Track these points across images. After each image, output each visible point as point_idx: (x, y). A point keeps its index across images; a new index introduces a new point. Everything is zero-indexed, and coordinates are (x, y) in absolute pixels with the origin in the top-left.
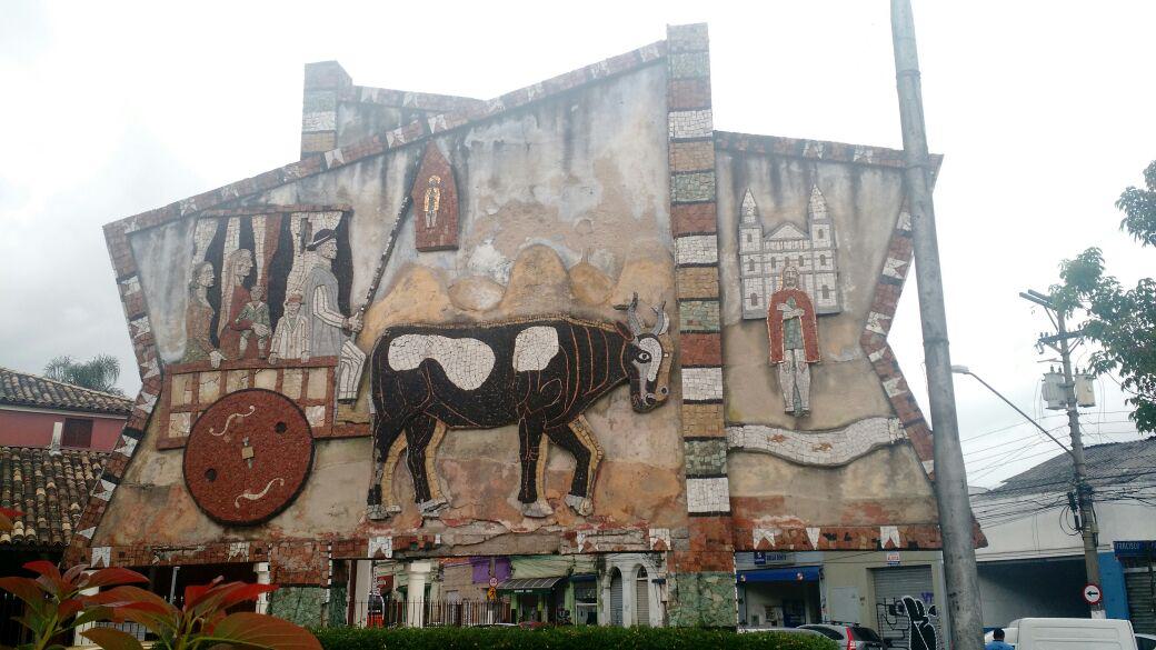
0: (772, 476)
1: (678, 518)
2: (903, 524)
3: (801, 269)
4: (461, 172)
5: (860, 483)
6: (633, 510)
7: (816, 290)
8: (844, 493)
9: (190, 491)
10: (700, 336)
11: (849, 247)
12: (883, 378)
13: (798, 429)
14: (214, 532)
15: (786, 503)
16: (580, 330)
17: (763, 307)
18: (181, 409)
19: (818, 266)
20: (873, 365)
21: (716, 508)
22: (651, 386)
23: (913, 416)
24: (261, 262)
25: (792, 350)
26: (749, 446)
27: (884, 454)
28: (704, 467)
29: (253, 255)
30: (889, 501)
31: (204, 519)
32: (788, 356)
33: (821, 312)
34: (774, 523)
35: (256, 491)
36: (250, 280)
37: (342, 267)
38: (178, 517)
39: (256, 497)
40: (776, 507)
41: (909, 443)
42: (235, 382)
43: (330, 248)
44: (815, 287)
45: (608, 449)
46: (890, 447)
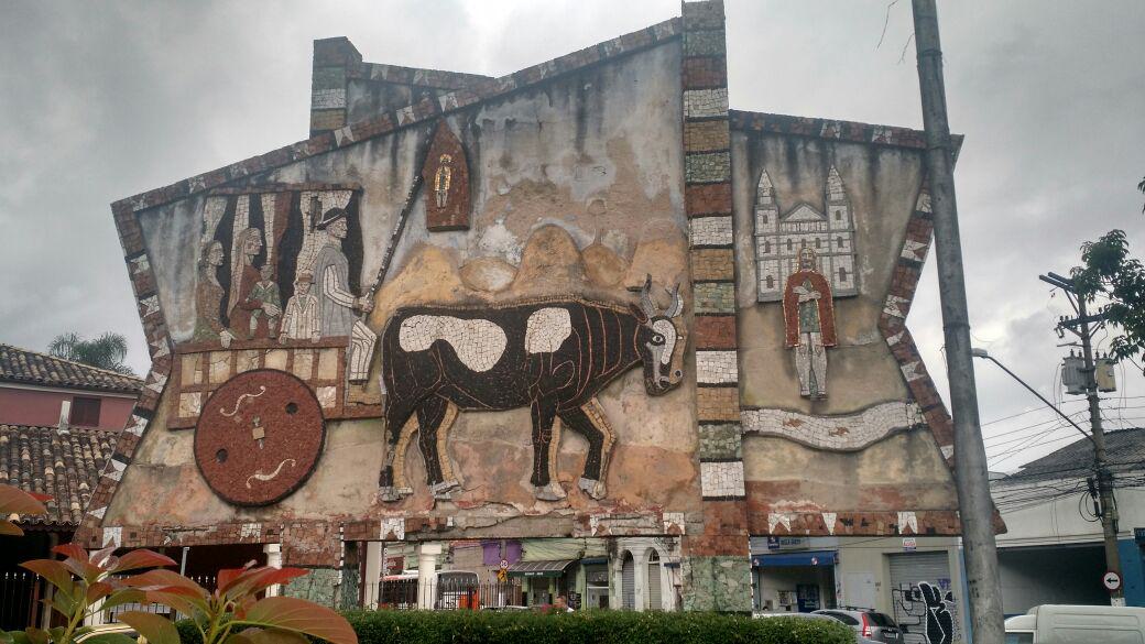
0: (788, 461)
2: (921, 510)
3: (818, 251)
6: (647, 494)
8: (860, 478)
9: (201, 471)
13: (814, 413)
14: (225, 513)
16: (592, 312)
17: (779, 289)
20: (891, 350)
21: (731, 493)
22: (665, 369)
23: (931, 401)
24: (270, 241)
26: (764, 430)
28: (718, 451)
29: (263, 234)
30: (907, 486)
31: (215, 500)
32: (804, 340)
33: (838, 295)
35: (267, 471)
36: (259, 259)
38: (190, 497)
39: (268, 478)
40: (792, 491)
42: (246, 363)
44: (832, 269)
46: (908, 432)
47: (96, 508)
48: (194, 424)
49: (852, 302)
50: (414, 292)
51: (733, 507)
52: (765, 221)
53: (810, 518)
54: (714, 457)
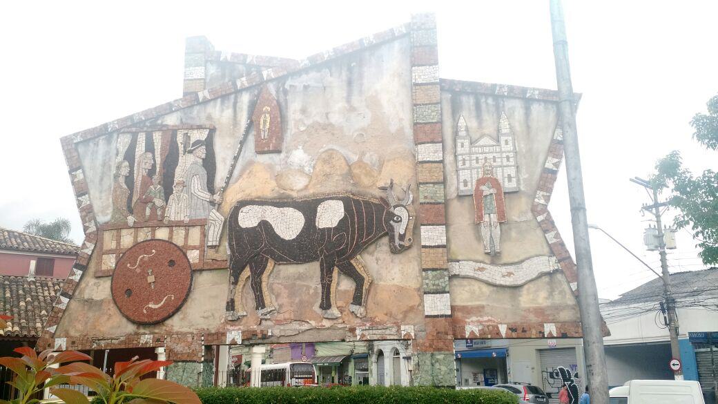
0: (477, 293)
1: (419, 319)
3: (495, 164)
4: (283, 104)
5: (531, 296)
7: (504, 178)
11: (524, 151)
12: (545, 231)
13: (493, 263)
14: (131, 328)
15: (486, 309)
17: (471, 188)
18: (110, 252)
19: (505, 163)
20: (540, 224)
22: (402, 237)
23: (564, 255)
24: (158, 160)
26: (463, 274)
27: (546, 279)
28: (435, 287)
31: (124, 320)
32: (486, 218)
34: (478, 321)
35: (157, 302)
36: (152, 172)
37: (209, 164)
38: (108, 319)
39: (157, 306)
40: (480, 312)
41: (562, 272)
42: (143, 235)
43: (201, 152)
44: (503, 175)
45: (375, 276)
47: (50, 326)
48: (111, 274)
49: (515, 194)
50: (247, 192)
51: (444, 321)
52: (462, 146)
53: (491, 327)
54: (432, 291)
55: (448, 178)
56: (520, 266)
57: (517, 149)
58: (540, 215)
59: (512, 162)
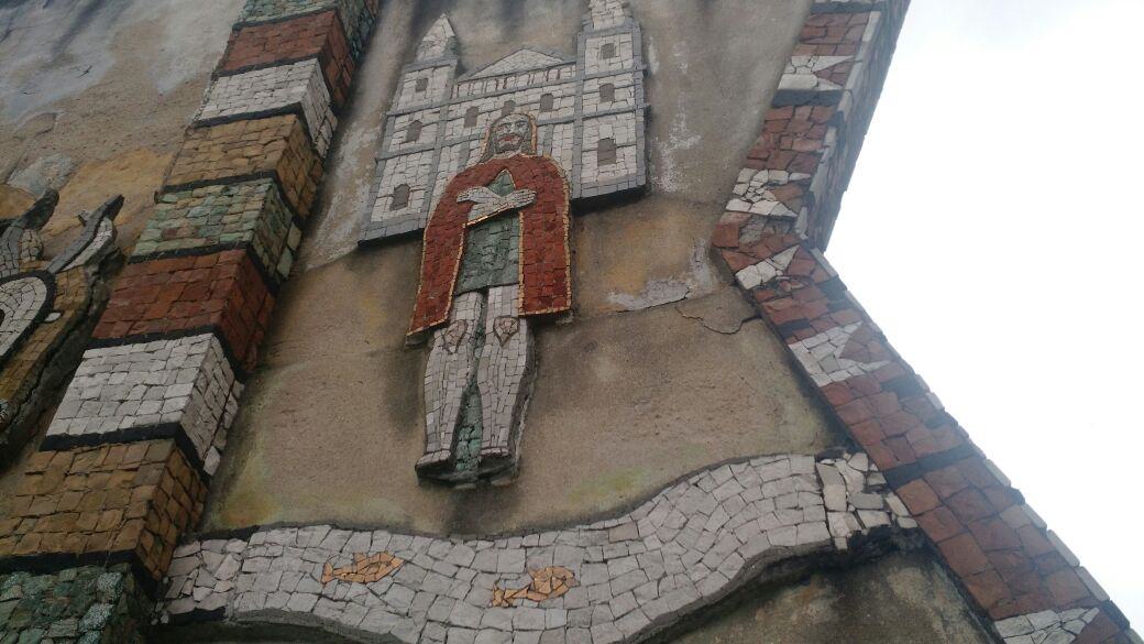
3: (545, 117)
10: (184, 262)
13: (460, 527)
17: (418, 210)
19: (592, 104)
25: (484, 292)
27: (809, 607)
32: (466, 309)
49: (631, 209)
55: (335, 201)
56: (623, 528)
57: (655, 67)
58: (758, 260)
59: (625, 98)
